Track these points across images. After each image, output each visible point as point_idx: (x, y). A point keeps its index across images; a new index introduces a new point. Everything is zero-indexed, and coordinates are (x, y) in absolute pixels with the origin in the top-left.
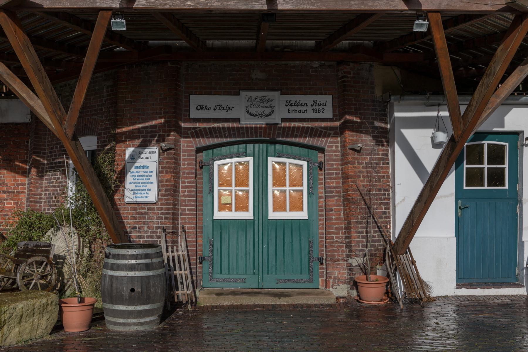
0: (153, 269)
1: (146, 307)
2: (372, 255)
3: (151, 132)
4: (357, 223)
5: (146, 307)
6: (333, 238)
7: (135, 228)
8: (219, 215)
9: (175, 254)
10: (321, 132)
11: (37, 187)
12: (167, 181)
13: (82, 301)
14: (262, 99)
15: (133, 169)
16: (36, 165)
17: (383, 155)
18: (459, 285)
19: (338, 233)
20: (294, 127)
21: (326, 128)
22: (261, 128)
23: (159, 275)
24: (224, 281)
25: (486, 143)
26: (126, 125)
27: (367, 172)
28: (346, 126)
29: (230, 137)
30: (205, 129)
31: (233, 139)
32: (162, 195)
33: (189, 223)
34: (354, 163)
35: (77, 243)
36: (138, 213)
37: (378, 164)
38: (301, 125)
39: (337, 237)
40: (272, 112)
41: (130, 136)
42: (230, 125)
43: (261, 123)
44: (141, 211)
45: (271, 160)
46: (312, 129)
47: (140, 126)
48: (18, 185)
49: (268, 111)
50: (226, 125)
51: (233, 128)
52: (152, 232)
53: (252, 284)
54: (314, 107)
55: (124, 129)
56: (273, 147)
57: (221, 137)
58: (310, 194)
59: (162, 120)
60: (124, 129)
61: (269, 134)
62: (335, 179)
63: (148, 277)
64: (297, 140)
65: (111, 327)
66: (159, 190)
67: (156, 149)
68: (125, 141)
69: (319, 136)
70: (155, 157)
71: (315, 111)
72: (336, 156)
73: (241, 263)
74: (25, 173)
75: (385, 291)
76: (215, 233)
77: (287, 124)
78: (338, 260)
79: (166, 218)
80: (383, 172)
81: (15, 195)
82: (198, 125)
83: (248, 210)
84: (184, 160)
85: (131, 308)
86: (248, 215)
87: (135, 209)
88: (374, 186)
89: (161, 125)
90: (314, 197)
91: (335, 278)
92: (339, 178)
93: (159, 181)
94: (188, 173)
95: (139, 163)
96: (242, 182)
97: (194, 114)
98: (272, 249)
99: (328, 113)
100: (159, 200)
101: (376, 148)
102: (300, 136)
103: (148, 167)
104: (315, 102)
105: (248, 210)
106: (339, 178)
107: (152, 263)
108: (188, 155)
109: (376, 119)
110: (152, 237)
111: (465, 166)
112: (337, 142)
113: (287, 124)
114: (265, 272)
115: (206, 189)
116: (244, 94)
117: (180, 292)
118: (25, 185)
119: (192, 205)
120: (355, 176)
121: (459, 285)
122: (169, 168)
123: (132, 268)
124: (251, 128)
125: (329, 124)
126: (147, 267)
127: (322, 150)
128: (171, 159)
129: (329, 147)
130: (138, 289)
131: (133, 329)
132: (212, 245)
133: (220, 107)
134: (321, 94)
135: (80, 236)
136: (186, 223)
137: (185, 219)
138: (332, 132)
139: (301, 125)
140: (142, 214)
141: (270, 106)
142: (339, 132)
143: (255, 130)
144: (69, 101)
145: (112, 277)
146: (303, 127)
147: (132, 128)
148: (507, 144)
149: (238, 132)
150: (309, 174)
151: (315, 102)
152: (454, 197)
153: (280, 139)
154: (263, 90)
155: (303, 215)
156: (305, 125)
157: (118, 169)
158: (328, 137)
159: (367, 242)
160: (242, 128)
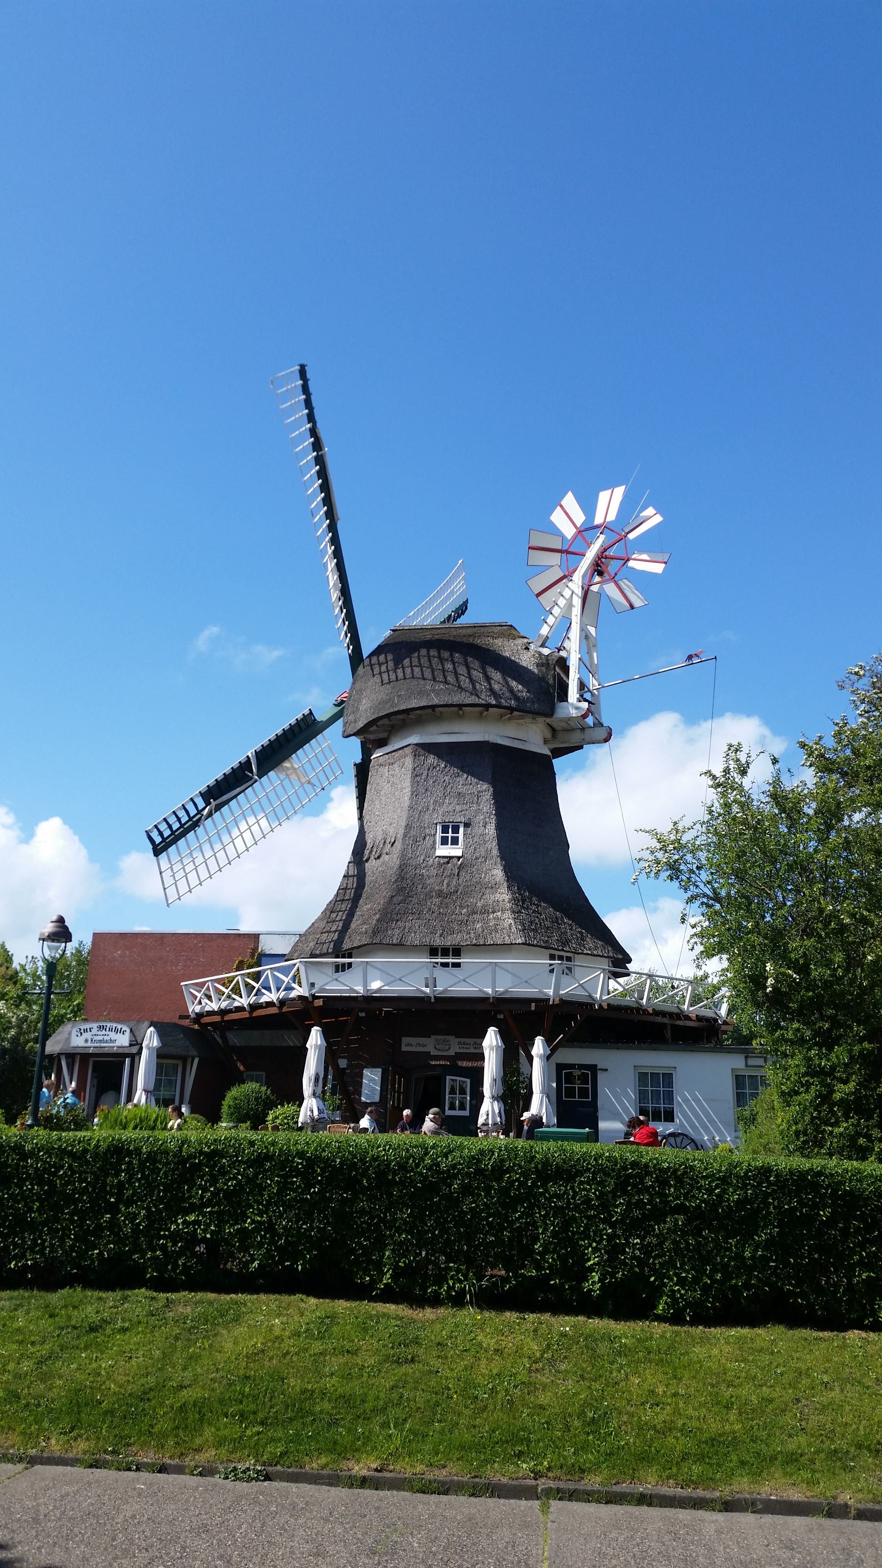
40: (450, 1048)
44: (445, 885)
71: (475, 1048)
75: (287, 821)
104: (475, 1043)
116: (433, 1037)
133: (420, 1045)
151: (475, 1043)
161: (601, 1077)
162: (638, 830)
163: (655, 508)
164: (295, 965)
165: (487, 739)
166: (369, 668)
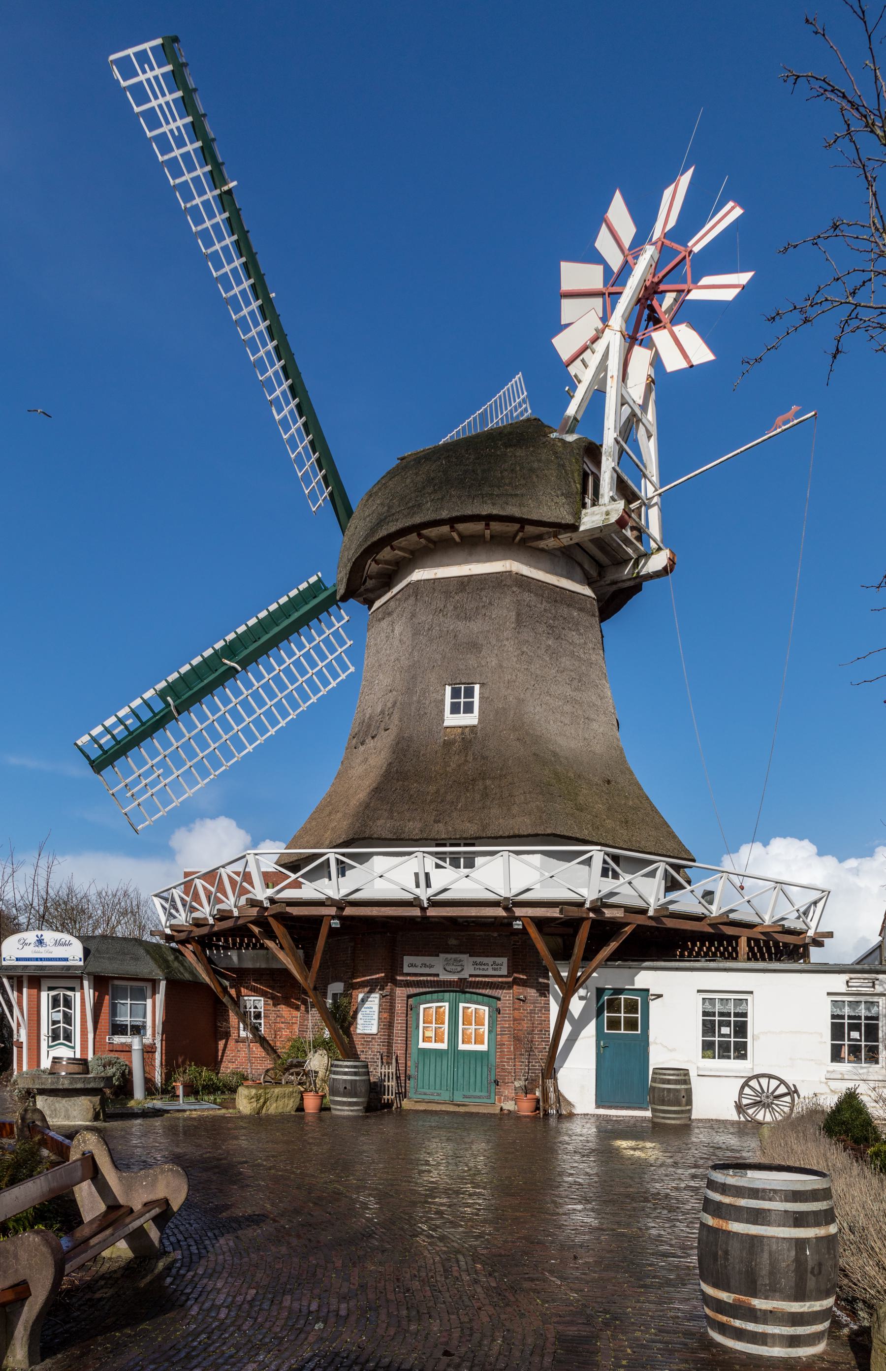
0: (359, 1076)
1: (354, 1100)
2: (532, 1080)
3: (375, 982)
4: (521, 1055)
5: (354, 1100)
6: (504, 1066)
7: (363, 1051)
8: (422, 1045)
9: (390, 1070)
10: (498, 985)
11: (305, 1020)
12: (385, 1018)
13: (316, 1092)
14: (455, 960)
15: (363, 1009)
16: (305, 1002)
17: (544, 1004)
18: (598, 1106)
19: (509, 1062)
20: (478, 981)
21: (502, 982)
22: (454, 981)
23: (364, 1080)
24: (425, 1094)
25: (622, 997)
26: (360, 977)
27: (531, 1016)
28: (517, 982)
29: (432, 988)
30: (413, 981)
31: (433, 989)
32: (381, 1029)
33: (400, 1050)
34: (520, 1010)
35: (326, 1062)
36: (365, 1041)
37: (541, 1011)
38: (484, 979)
39: (508, 1065)
41: (362, 985)
42: (432, 978)
43: (455, 977)
45: (461, 1005)
46: (492, 982)
47: (369, 978)
48: (293, 1017)
49: (459, 969)
50: (429, 978)
51: (434, 981)
52: (374, 1055)
53: (446, 1096)
54: (494, 966)
55: (358, 980)
56: (463, 995)
57: (425, 987)
58: (490, 1032)
59: (383, 975)
60: (358, 980)
61: (460, 986)
62: (507, 1021)
63: (356, 1080)
64: (480, 991)
65: (334, 1112)
66: (379, 1025)
67: (377, 995)
68: (358, 988)
69: (497, 989)
70: (377, 1001)
71: (494, 969)
72: (509, 1004)
73: (444, 1082)
74: (297, 1008)
76: (420, 1058)
77: (473, 979)
78: (508, 1083)
79: (383, 1045)
80: (545, 1017)
81: (290, 1025)
82: (409, 978)
83: (443, 1042)
84: (398, 1003)
85: (345, 1099)
86: (444, 1046)
87: (364, 1038)
88: (536, 1027)
89: (382, 978)
90: (493, 1034)
91: (505, 1096)
92: (510, 1021)
93: (379, 1019)
94: (401, 1013)
95: (367, 1005)
96: (440, 1020)
97: (406, 970)
98: (460, 1071)
99: (504, 972)
100: (379, 1032)
101: (539, 998)
102: (483, 989)
103: (372, 1008)
104: (494, 962)
105: (443, 1042)
106: (510, 1021)
107: (359, 1072)
108: (402, 1000)
109: (540, 977)
110: (374, 1059)
111: (606, 1014)
112: (510, 993)
113: (473, 979)
114: (455, 1089)
115: (414, 1026)
116: (442, 956)
117: (386, 1097)
118: (297, 1017)
119: (403, 1037)
120: (520, 1020)
121: (598, 1106)
122: (386, 1009)
123: (346, 1074)
124: (447, 981)
125: (504, 979)
126: (355, 1074)
127: (499, 999)
128: (387, 1002)
129: (504, 997)
130: (349, 1087)
131: (346, 1113)
132: (417, 1067)
133: (425, 965)
134: (499, 956)
135: (329, 1057)
136: (398, 1050)
137: (397, 1047)
138: (507, 986)
139: (484, 979)
140: (368, 1041)
141: (461, 965)
142: (509, 986)
143: (450, 983)
144: (311, 967)
145: (334, 1079)
146: (485, 981)
147: (363, 979)
148: (639, 999)
149: (438, 984)
150: (490, 1016)
151: (494, 962)
152: (594, 1039)
153: (468, 990)
154: (456, 953)
155: (484, 1047)
156: (487, 979)
157: (353, 1008)
158: (504, 989)
159: (529, 1069)
160: (441, 981)
161: (653, 1005)
162: (778, 318)
163: (734, 201)
164: (228, 875)
165: (508, 569)
166: (423, 1200)
